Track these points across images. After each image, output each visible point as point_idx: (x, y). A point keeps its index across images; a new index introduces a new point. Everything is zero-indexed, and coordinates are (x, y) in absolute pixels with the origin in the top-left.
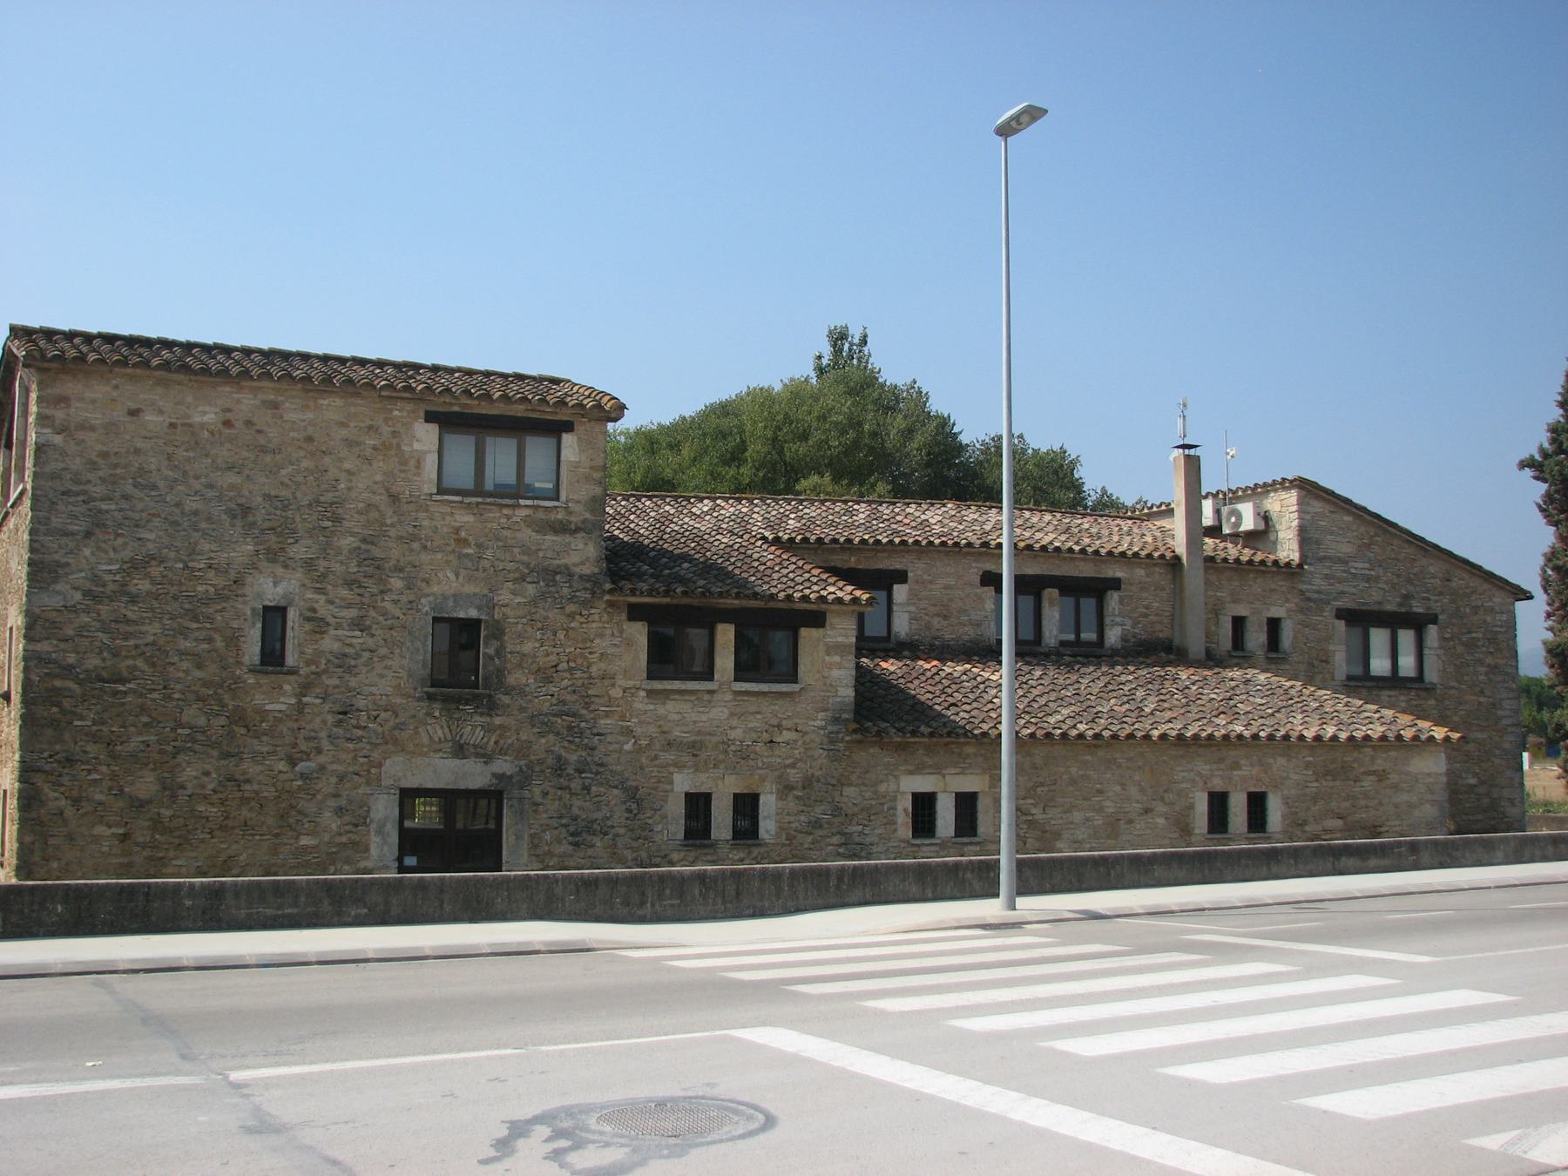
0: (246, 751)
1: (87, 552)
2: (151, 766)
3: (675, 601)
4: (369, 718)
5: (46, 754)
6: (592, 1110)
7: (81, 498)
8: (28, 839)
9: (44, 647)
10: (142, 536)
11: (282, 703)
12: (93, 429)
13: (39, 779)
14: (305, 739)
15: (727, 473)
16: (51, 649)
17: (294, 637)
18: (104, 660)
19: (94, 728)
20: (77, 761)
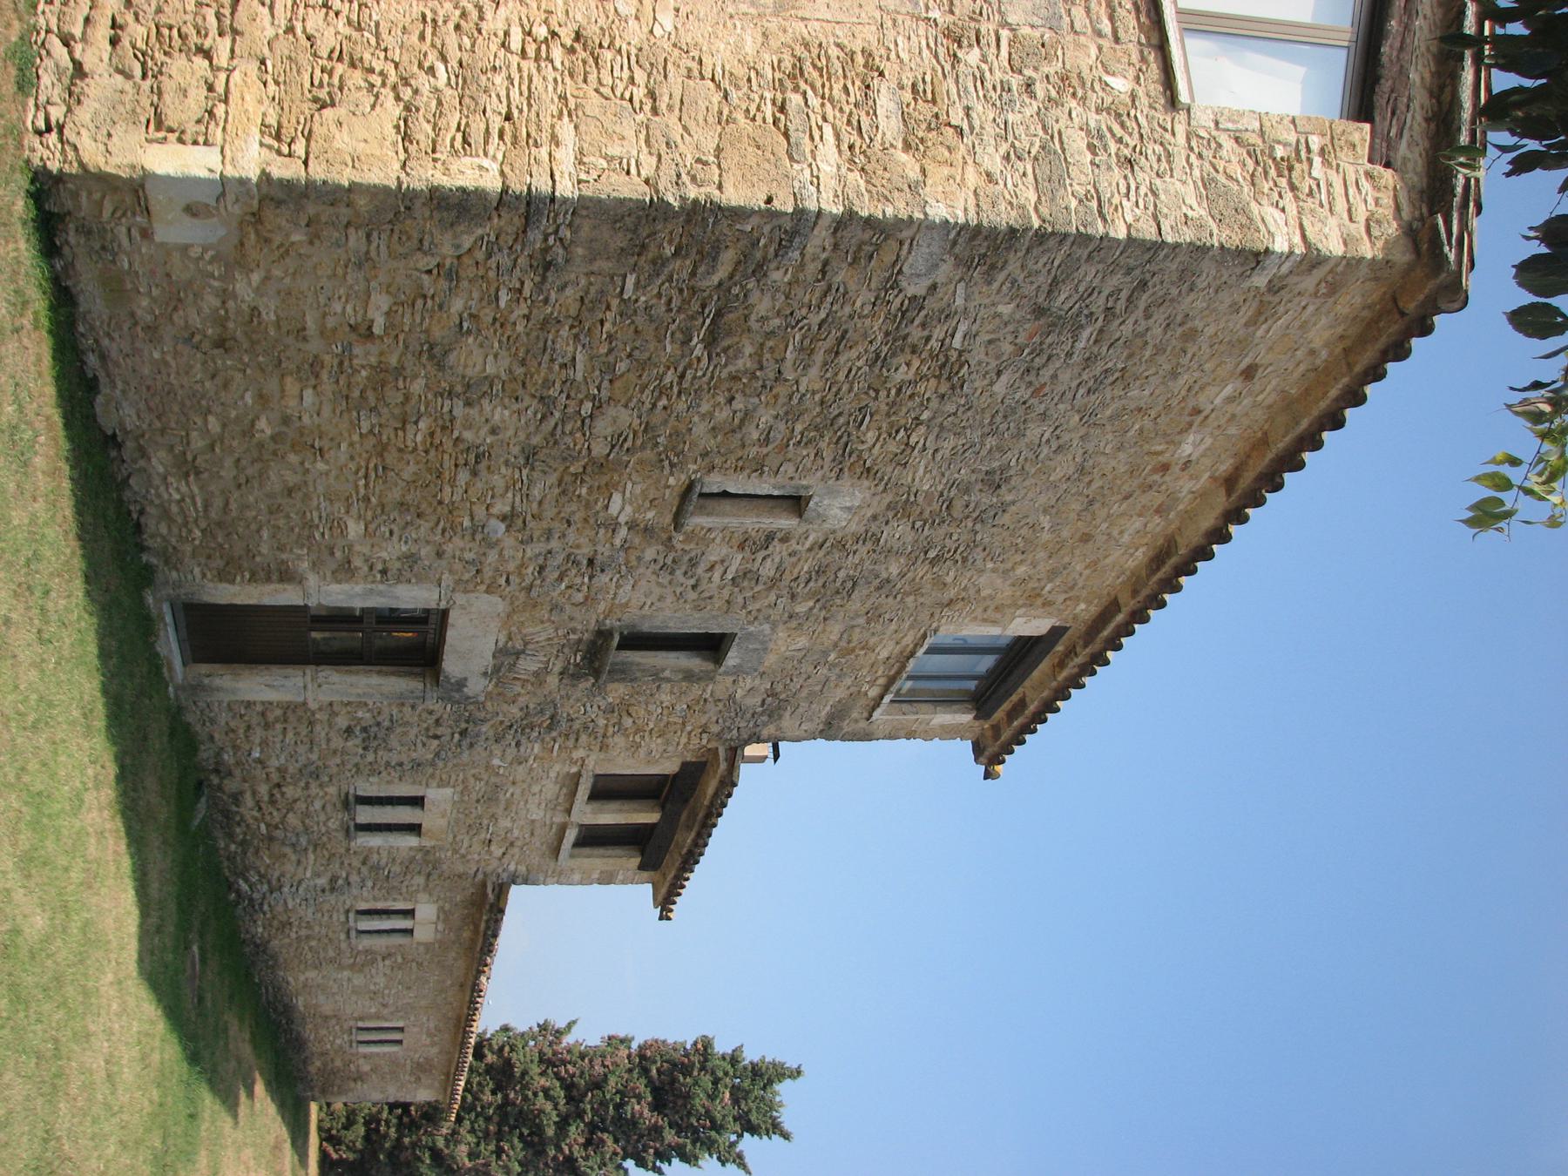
0: (535, 474)
1: (1005, 309)
2: (519, 371)
3: (1027, 683)
4: (153, 395)
5: (566, 233)
6: (184, 739)
7: (1121, 305)
8: (362, 202)
9: (820, 237)
10: (1004, 378)
11: (623, 509)
12: (1253, 322)
13: (509, 222)
14: (550, 530)
15: (1012, 386)
16: (810, 250)
17: (643, 388)
18: (763, 319)
19: (615, 303)
20: (544, 278)
